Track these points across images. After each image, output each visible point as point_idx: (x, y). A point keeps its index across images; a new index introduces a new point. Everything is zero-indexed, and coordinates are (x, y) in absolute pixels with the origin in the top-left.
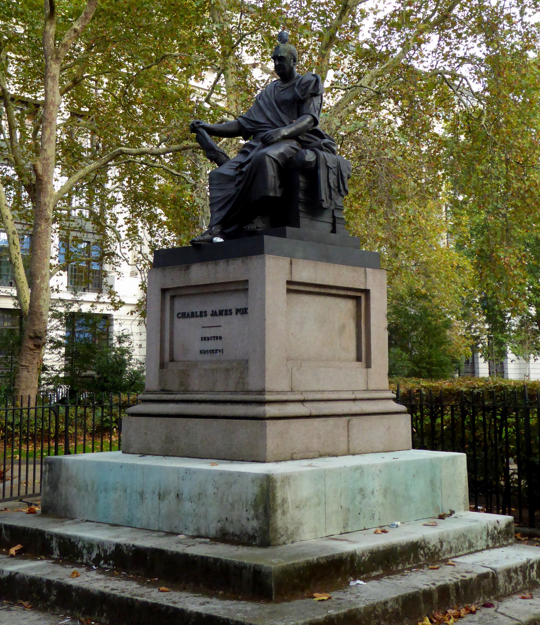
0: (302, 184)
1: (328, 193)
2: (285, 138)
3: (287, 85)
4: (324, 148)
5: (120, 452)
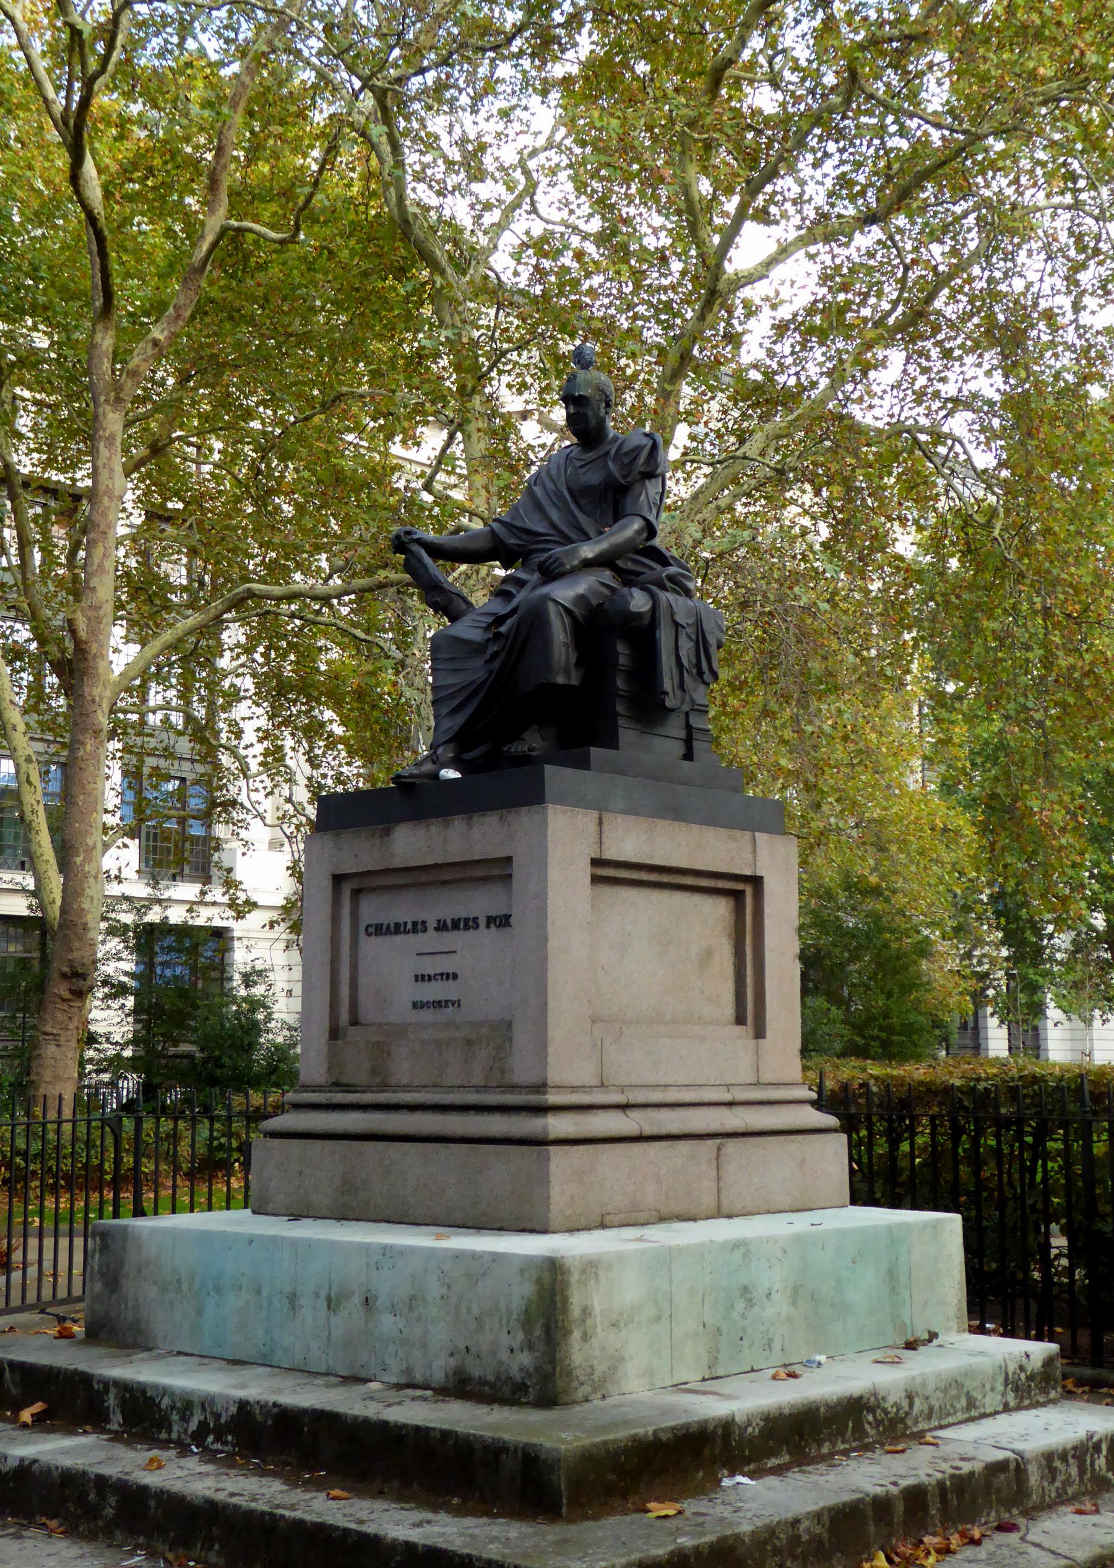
0: (622, 660)
1: (676, 678)
2: (588, 564)
3: (591, 455)
4: (668, 584)
5: (248, 1211)
